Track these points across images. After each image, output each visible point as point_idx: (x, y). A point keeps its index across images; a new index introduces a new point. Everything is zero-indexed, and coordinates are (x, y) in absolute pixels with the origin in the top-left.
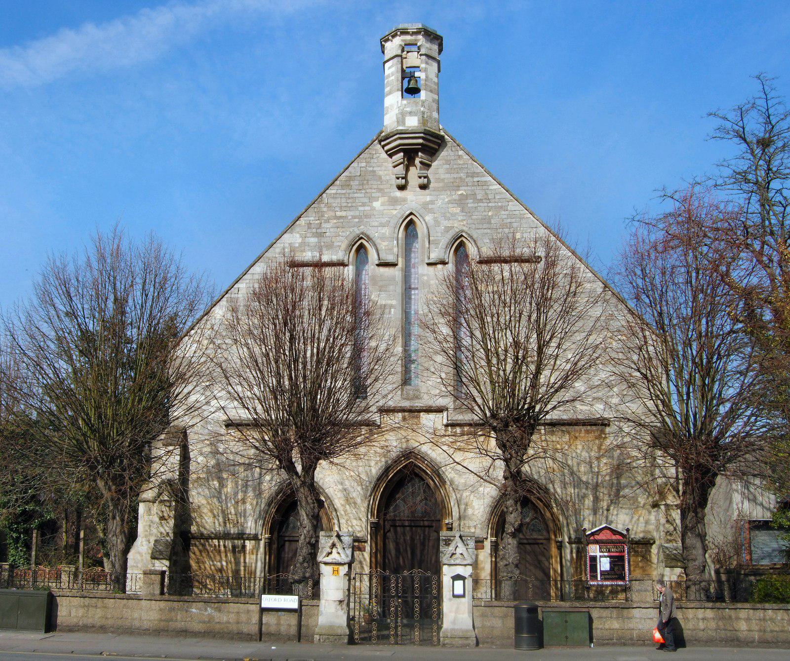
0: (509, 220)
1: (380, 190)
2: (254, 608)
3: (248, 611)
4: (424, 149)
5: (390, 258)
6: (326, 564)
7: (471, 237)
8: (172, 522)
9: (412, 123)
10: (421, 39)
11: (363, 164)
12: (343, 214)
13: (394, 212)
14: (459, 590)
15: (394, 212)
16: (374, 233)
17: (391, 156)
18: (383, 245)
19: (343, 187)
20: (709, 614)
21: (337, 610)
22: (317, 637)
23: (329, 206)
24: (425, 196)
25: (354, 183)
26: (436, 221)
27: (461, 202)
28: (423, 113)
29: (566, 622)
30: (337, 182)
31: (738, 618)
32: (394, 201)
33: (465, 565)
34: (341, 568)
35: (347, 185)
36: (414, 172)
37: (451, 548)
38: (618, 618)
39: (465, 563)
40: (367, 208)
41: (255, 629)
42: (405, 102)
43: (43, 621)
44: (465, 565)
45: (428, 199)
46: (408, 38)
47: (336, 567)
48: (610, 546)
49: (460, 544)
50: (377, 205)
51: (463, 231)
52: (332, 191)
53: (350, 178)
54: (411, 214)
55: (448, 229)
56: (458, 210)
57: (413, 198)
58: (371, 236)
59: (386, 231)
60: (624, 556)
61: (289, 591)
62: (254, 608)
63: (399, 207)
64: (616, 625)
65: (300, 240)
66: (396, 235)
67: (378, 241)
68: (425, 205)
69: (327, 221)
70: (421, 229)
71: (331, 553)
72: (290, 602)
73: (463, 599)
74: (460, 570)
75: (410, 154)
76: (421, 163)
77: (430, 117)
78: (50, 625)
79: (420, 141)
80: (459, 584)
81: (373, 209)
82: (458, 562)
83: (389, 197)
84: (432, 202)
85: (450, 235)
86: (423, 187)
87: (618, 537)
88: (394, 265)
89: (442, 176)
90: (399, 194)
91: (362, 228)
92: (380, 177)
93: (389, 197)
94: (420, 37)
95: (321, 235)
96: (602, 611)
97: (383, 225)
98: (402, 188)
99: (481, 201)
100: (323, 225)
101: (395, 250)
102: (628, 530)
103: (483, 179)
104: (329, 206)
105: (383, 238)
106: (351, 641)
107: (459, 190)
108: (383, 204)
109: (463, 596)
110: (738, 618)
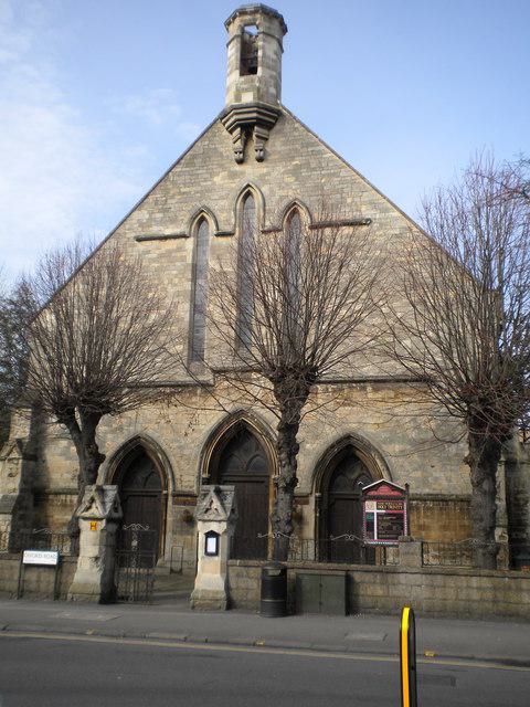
0: (341, 186)
1: (221, 166)
2: (17, 563)
3: (12, 568)
4: (260, 123)
5: (228, 229)
6: (85, 519)
7: (304, 204)
8: (18, 479)
9: (248, 98)
10: (259, 18)
11: (206, 143)
12: (187, 189)
13: (234, 185)
14: (212, 548)
15: (234, 185)
16: (214, 206)
17: (231, 132)
18: (222, 217)
19: (187, 165)
20: (486, 582)
21: (92, 568)
22: (70, 595)
23: (174, 183)
24: (262, 169)
25: (198, 161)
26: (272, 191)
27: (295, 172)
28: (259, 89)
29: (321, 586)
30: (183, 161)
31: (519, 589)
32: (233, 175)
33: (220, 521)
34: (99, 523)
35: (190, 164)
36: (254, 143)
37: (205, 503)
38: (382, 584)
39: (219, 518)
40: (209, 183)
41: (13, 586)
42: (243, 79)
43: (342, 602)
44: (220, 521)
45: (265, 170)
46: (247, 17)
47: (94, 523)
48: (388, 503)
49: (215, 500)
50: (217, 179)
51: (296, 199)
52: (178, 169)
53: (194, 157)
54: (248, 186)
55: (282, 198)
56: (292, 179)
57: (252, 171)
58: (212, 209)
59: (225, 203)
60: (402, 515)
61: (47, 547)
62: (17, 563)
63: (237, 180)
64: (380, 591)
65: (147, 216)
66: (233, 207)
67: (217, 213)
68: (262, 178)
69: (172, 197)
70: (257, 199)
71: (90, 508)
72: (49, 558)
73: (216, 558)
74: (214, 527)
75: (246, 129)
76: (257, 136)
77: (267, 92)
78: (351, 608)
79: (255, 115)
80: (212, 541)
81: (214, 183)
82: (212, 517)
83: (229, 171)
84: (269, 174)
85: (285, 203)
86: (260, 160)
87: (396, 493)
88: (230, 234)
89: (279, 149)
90: (238, 168)
91: (204, 202)
92: (221, 153)
93: (229, 171)
94: (258, 16)
95: (165, 211)
96: (365, 574)
97: (222, 198)
98: (240, 162)
99: (314, 169)
100: (169, 201)
101: (233, 220)
102: (407, 486)
103: (318, 148)
104: (174, 183)
105: (222, 210)
106: (231, 605)
107: (293, 160)
108: (223, 178)
109: (216, 554)
110: (519, 589)
